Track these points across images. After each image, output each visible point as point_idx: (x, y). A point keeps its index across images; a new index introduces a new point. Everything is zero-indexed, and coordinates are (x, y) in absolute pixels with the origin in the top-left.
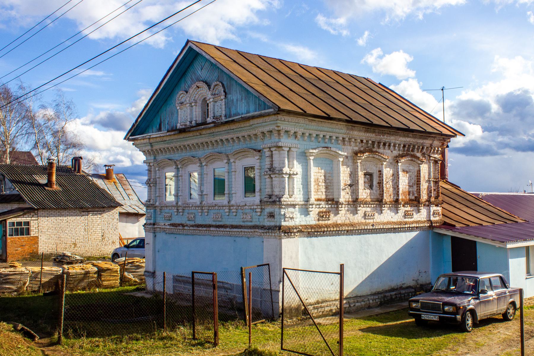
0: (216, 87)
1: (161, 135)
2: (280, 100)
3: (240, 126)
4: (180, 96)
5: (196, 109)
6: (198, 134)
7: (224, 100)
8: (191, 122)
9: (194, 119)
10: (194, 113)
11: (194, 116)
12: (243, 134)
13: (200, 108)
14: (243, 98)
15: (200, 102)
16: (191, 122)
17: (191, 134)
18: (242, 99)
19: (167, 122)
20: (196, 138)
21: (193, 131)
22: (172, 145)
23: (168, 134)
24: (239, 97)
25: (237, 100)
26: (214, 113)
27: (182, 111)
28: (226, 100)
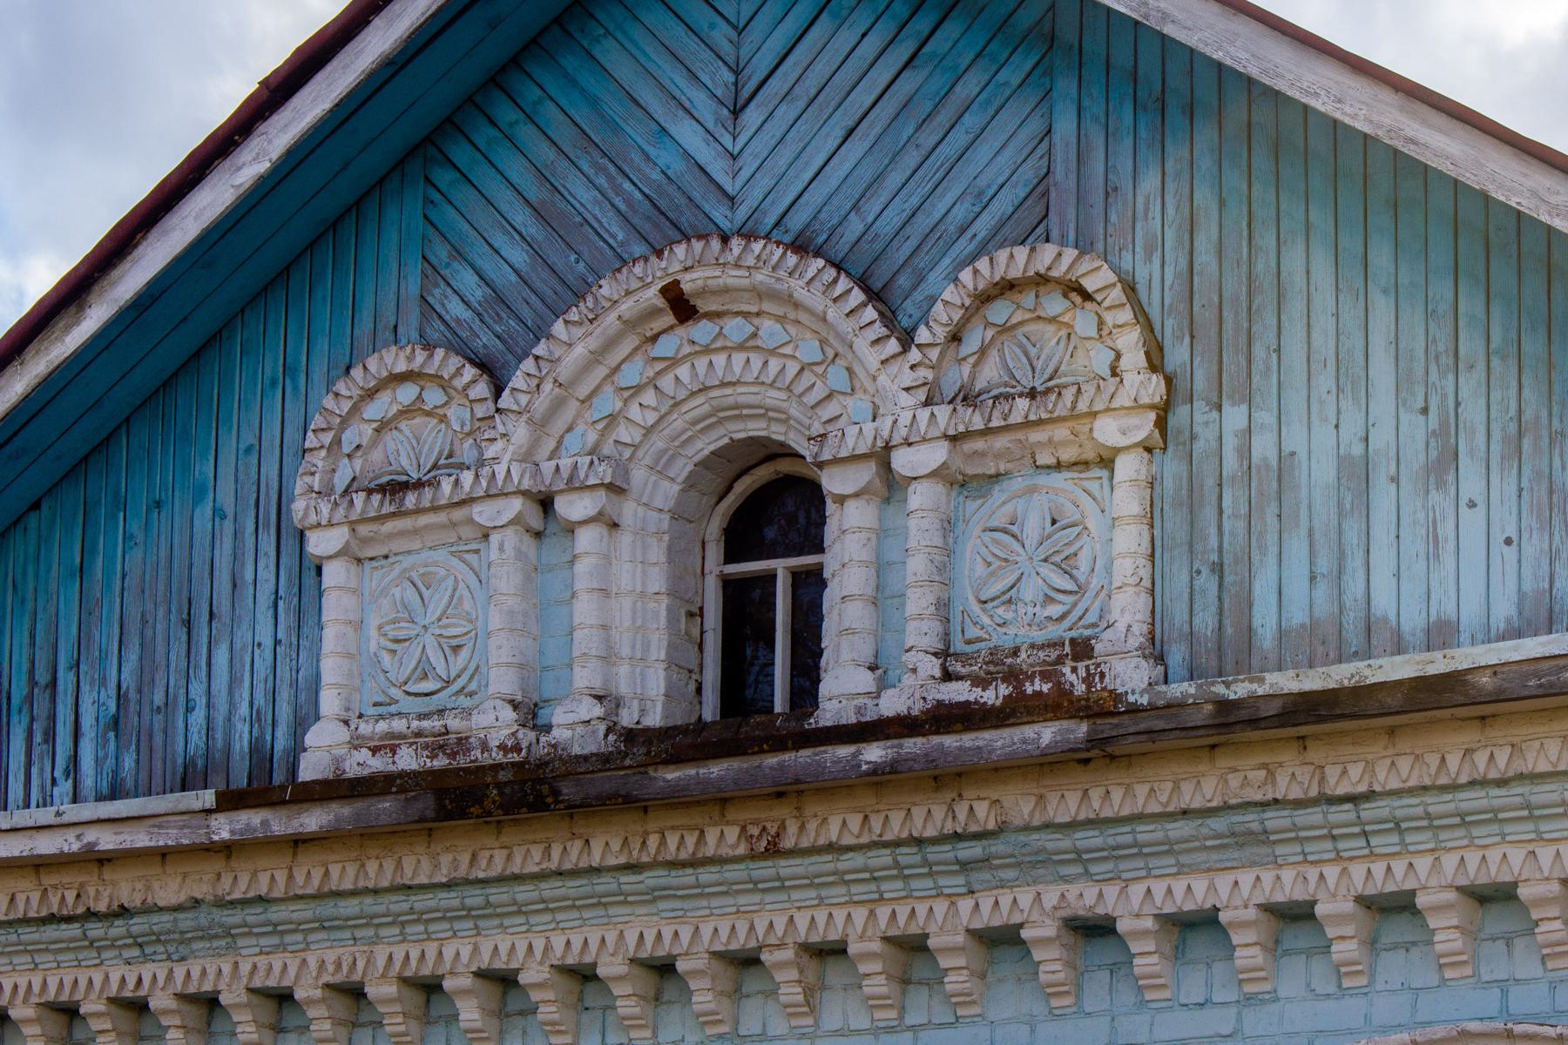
0: (1000, 312)
1: (107, 840)
2: (66, 691)
3: (574, 856)
4: (375, 405)
5: (607, 560)
6: (724, 837)
7: (1128, 467)
8: (531, 713)
9: (586, 677)
10: (585, 610)
11: (586, 641)
12: (500, 945)
13: (657, 553)
14: (1471, 445)
15: (667, 493)
16: (531, 713)
17: (605, 845)
18: (1444, 463)
19: (95, 705)
20: (653, 896)
21: (679, 801)
22: (206, 970)
23: (223, 828)
24: (1395, 430)
25: (1357, 474)
26: (943, 608)
27: (374, 578)
28: (1171, 467)
